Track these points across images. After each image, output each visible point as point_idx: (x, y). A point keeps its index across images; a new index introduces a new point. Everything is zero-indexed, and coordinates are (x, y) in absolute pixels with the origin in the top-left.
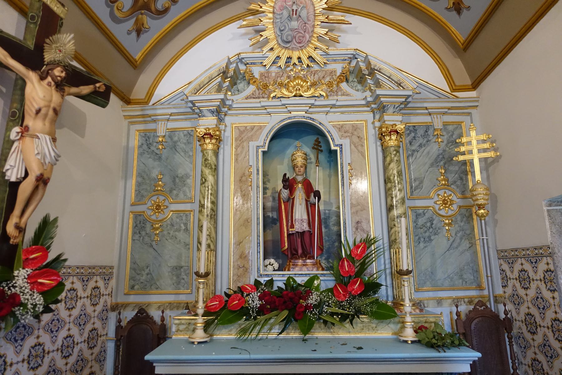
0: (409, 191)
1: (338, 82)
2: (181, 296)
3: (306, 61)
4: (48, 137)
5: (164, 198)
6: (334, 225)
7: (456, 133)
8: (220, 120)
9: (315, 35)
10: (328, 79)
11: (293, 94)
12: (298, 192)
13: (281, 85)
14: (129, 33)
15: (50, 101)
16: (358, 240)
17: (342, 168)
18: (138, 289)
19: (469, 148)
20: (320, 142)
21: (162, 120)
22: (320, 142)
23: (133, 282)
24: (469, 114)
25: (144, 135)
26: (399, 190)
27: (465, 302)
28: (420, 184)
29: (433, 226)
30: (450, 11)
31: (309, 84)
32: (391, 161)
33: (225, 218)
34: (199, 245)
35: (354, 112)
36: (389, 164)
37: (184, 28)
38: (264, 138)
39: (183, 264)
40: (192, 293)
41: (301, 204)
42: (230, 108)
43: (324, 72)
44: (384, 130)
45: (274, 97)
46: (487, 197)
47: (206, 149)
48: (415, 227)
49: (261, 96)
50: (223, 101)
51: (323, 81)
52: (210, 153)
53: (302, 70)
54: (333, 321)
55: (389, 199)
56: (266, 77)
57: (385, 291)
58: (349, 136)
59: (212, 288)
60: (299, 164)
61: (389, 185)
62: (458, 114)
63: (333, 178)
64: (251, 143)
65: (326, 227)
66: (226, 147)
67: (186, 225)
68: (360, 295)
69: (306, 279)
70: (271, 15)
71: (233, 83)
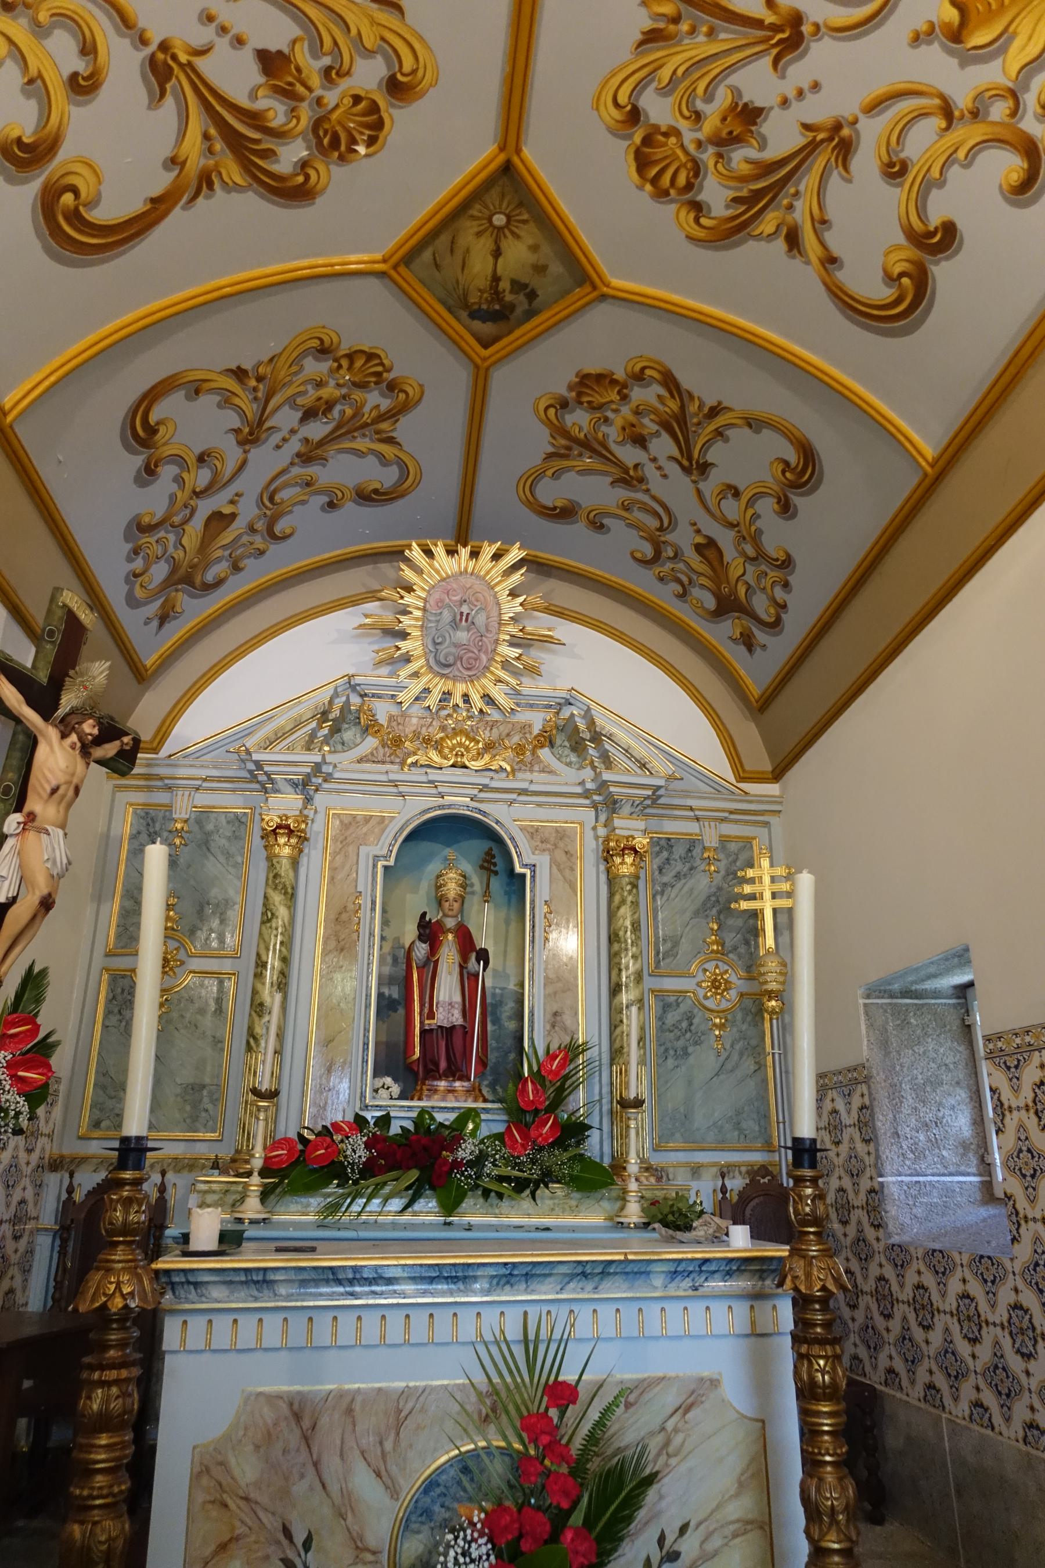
0: (652, 961)
1: (535, 747)
2: (199, 1144)
5: (176, 944)
6: (510, 1018)
7: (743, 857)
8: (308, 800)
10: (516, 739)
12: (447, 950)
13: (427, 741)
15: (73, 775)
16: (554, 1047)
17: (533, 909)
20: (494, 857)
22: (494, 857)
23: (98, 1112)
24: (766, 824)
25: (143, 814)
26: (633, 957)
27: (740, 1173)
28: (673, 947)
29: (693, 1028)
30: (738, 644)
31: (480, 745)
32: (623, 902)
34: (252, 1041)
35: (555, 804)
36: (618, 908)
37: (244, 610)
39: (207, 1080)
40: (221, 1141)
41: (450, 973)
43: (510, 726)
44: (612, 844)
45: (414, 764)
46: (781, 979)
47: (277, 856)
48: (661, 1029)
49: (388, 759)
50: (317, 767)
51: (506, 742)
53: (469, 718)
55: (615, 972)
56: (399, 724)
57: (598, 1147)
58: (549, 850)
60: (452, 895)
61: (616, 947)
62: (746, 822)
63: (513, 926)
65: (494, 1023)
68: (552, 1145)
69: (452, 1116)
70: (418, 613)
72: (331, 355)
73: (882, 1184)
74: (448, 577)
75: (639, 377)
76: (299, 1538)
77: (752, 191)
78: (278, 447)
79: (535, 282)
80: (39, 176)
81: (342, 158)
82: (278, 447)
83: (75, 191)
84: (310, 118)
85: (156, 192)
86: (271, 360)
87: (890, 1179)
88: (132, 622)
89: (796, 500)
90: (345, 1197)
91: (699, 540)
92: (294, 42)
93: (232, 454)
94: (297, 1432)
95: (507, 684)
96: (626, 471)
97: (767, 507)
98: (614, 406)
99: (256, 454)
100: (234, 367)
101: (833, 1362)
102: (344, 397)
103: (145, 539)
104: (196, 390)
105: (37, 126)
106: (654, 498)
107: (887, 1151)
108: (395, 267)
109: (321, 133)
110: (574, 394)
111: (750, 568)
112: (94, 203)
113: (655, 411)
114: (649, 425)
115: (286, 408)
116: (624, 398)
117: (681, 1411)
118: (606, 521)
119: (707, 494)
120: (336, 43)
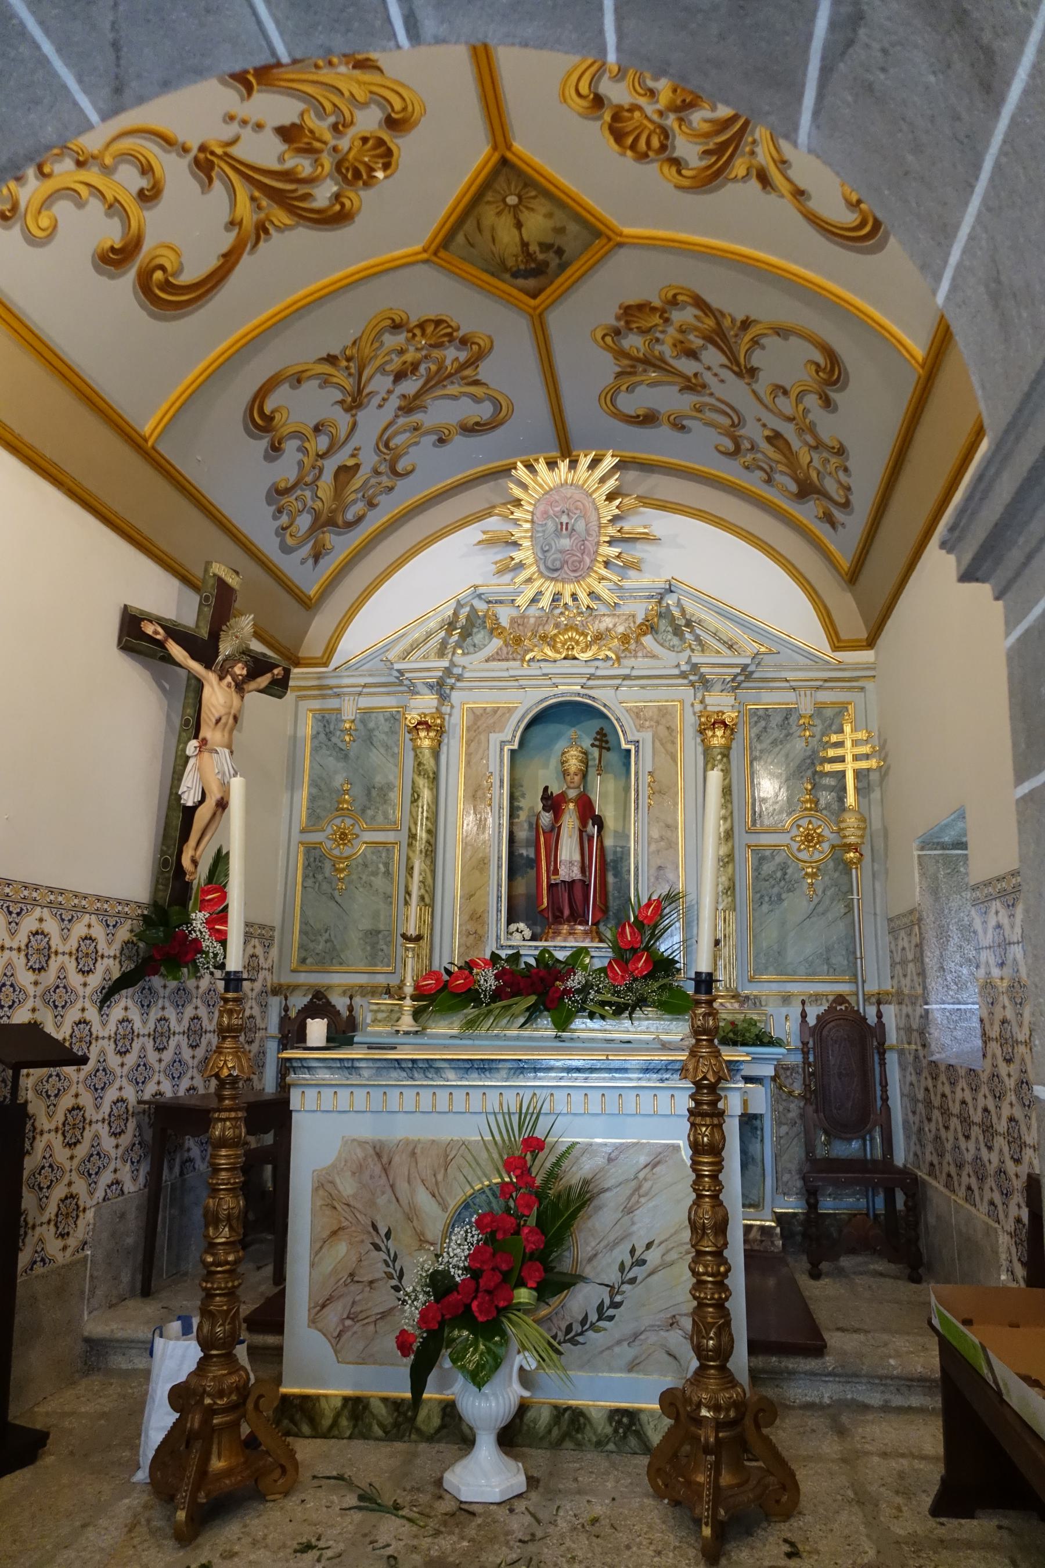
3: (584, 599)
4: (227, 751)
5: (352, 822)
8: (443, 698)
9: (600, 559)
11: (563, 656)
13: (544, 638)
14: (303, 561)
15: (231, 707)
16: (655, 897)
18: (312, 964)
19: (839, 752)
21: (349, 694)
24: (862, 689)
29: (787, 877)
31: (589, 638)
33: (448, 856)
37: (381, 541)
38: (513, 728)
39: (382, 927)
41: (571, 837)
42: (460, 677)
44: (703, 720)
45: (532, 660)
46: (859, 833)
47: (420, 747)
48: (756, 879)
50: (448, 671)
52: (427, 752)
54: (603, 1013)
59: (426, 962)
60: (573, 769)
64: (493, 736)
65: (615, 876)
66: (452, 742)
67: (386, 865)
68: (644, 977)
69: (568, 953)
71: (466, 633)
72: (404, 329)
73: (927, 1011)
74: (551, 490)
75: (673, 302)
76: (383, 1231)
77: (716, 144)
78: (380, 406)
79: (559, 241)
80: (130, 269)
81: (365, 184)
82: (380, 406)
83: (162, 268)
84: (332, 164)
85: (225, 249)
86: (354, 343)
87: (934, 1006)
88: (292, 565)
89: (833, 395)
90: (478, 1016)
91: (767, 433)
92: (302, 115)
93: (342, 420)
94: (379, 1166)
95: (610, 580)
96: (688, 379)
97: (812, 401)
98: (660, 328)
99: (361, 415)
100: (325, 355)
101: (712, 1129)
102: (426, 357)
103: (284, 500)
104: (298, 380)
105: (123, 232)
106: (719, 400)
107: (933, 984)
108: (435, 254)
109: (344, 171)
110: (622, 323)
111: (815, 456)
112: (180, 270)
113: (696, 329)
114: (696, 341)
115: (378, 376)
116: (667, 320)
117: (649, 1167)
118: (685, 422)
119: (762, 394)
120: (335, 105)
